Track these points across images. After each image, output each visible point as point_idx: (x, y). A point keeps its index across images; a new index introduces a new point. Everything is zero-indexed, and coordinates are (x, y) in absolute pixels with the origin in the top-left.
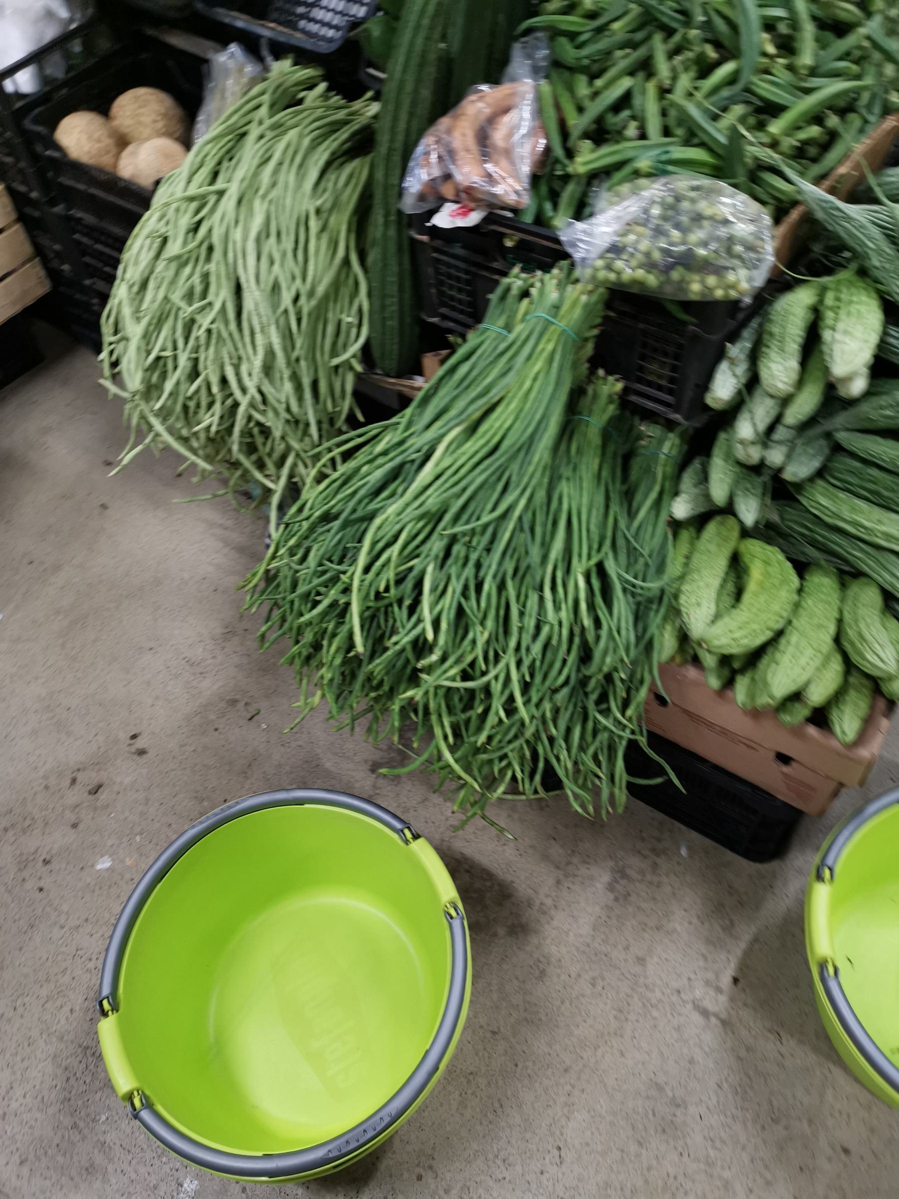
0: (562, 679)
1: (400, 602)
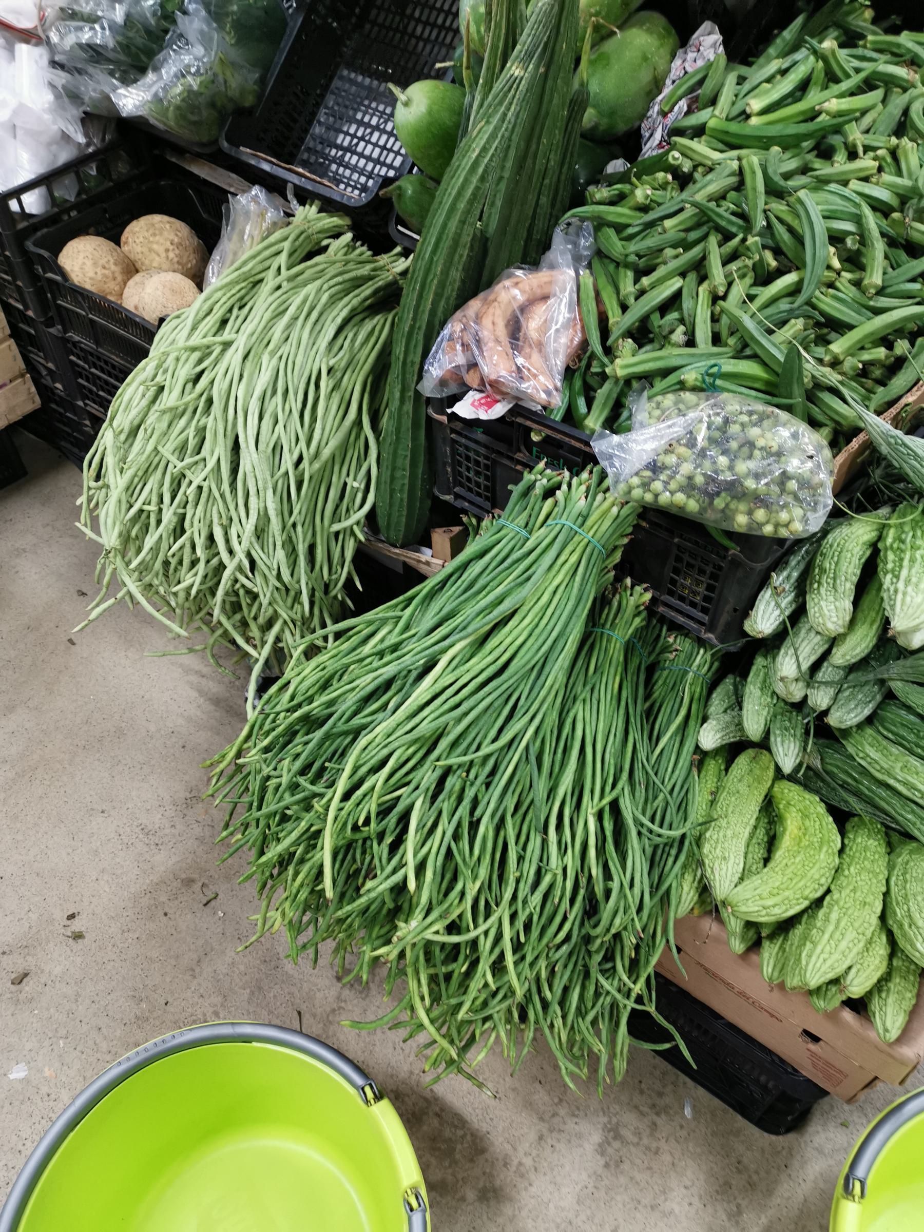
0: (562, 935)
1: (381, 836)
